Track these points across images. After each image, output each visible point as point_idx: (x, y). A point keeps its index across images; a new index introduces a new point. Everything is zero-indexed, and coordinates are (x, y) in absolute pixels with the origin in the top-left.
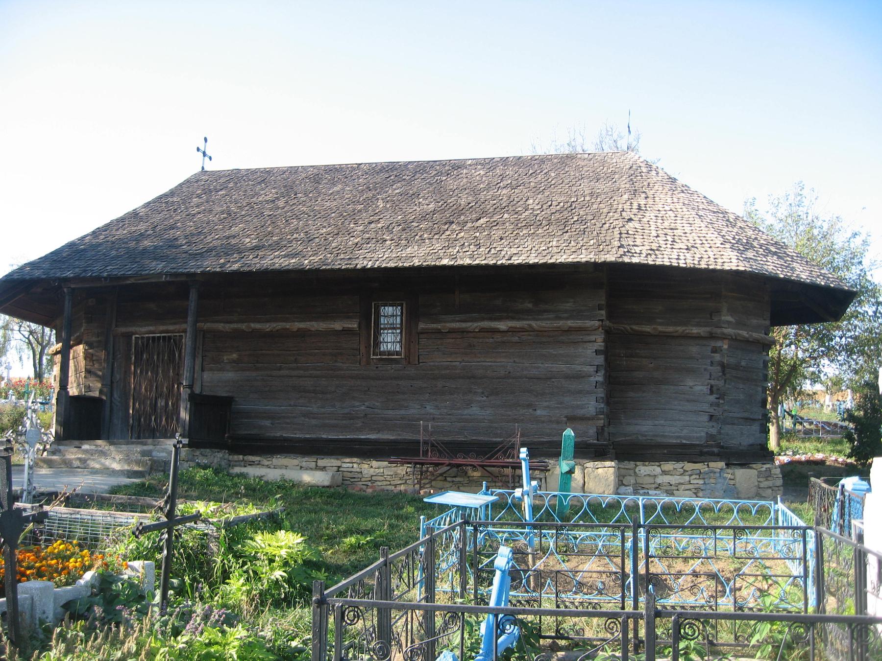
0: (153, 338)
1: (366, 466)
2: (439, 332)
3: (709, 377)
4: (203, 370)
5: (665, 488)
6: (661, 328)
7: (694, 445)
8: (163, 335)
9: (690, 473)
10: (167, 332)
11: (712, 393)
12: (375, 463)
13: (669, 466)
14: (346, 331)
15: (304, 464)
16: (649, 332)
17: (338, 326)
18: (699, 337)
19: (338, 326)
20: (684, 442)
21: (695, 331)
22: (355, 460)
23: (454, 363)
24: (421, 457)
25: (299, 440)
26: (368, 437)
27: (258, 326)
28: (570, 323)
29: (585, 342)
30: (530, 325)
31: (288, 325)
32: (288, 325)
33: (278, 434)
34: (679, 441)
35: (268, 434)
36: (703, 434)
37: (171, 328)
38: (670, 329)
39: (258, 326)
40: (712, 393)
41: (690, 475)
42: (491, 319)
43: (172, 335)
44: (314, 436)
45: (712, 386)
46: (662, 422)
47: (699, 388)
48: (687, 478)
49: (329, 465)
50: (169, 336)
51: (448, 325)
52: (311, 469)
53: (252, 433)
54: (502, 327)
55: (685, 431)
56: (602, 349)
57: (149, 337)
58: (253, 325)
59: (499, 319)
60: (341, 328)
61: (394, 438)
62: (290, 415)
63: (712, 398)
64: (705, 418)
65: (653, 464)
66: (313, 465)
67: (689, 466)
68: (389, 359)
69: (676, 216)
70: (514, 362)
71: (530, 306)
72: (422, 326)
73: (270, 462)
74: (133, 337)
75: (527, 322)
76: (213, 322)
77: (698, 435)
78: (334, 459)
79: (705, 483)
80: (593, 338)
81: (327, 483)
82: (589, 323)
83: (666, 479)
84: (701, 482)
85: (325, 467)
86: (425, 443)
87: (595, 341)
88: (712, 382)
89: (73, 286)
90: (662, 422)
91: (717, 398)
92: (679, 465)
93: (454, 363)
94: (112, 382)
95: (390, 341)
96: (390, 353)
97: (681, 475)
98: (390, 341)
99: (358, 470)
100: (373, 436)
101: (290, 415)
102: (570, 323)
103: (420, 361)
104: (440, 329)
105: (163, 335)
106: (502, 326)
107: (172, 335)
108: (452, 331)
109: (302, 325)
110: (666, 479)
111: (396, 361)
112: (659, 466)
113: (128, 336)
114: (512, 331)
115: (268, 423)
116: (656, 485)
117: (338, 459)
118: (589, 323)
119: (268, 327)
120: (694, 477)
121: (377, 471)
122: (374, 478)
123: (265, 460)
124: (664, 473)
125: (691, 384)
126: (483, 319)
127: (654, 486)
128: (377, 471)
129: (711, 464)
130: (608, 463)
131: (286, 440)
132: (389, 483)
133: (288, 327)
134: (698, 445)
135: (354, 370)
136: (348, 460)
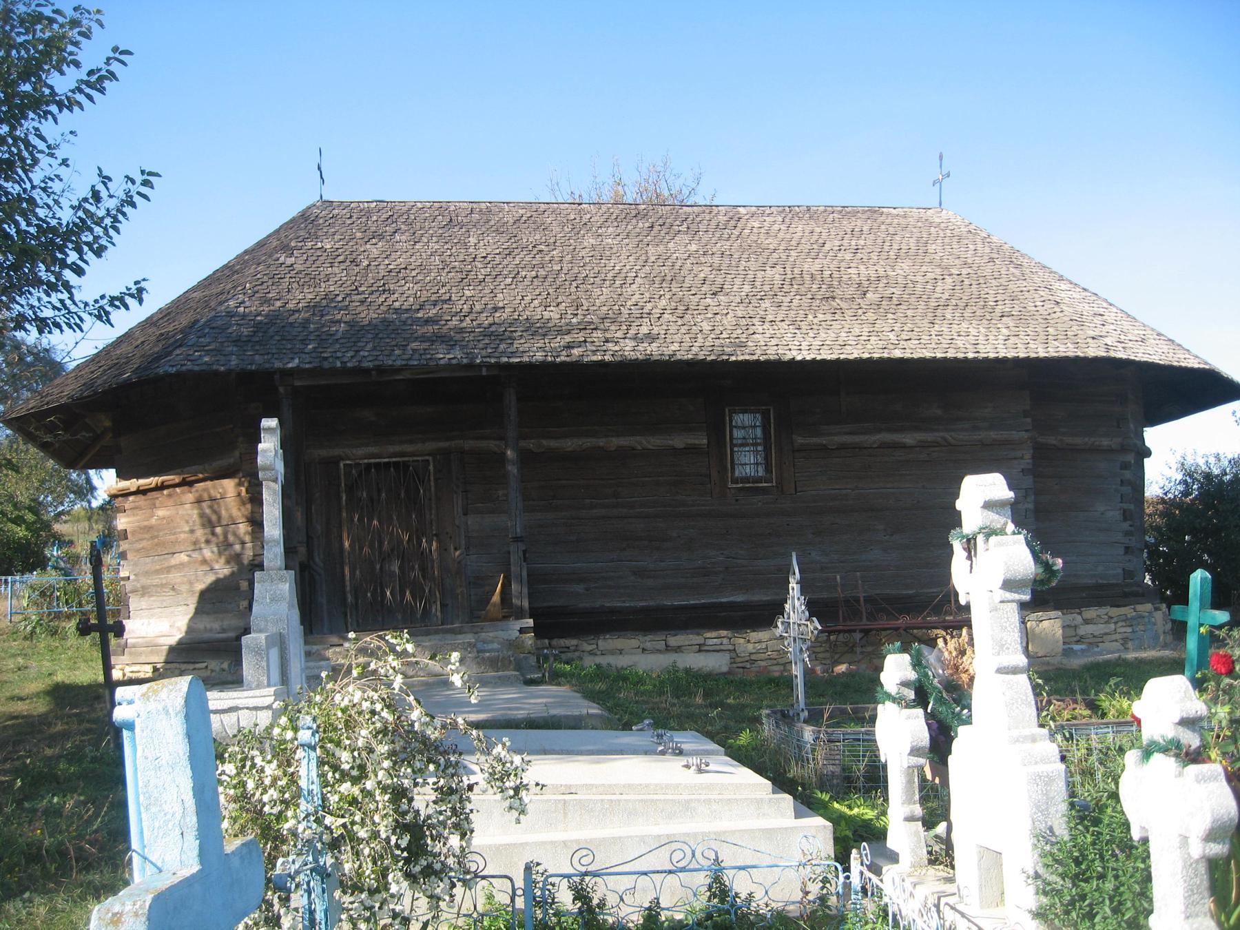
0: (377, 465)
1: (742, 641)
2: (824, 448)
3: (1120, 500)
4: (465, 514)
5: (1087, 640)
6: (1069, 440)
7: (1112, 585)
8: (394, 460)
9: (1115, 620)
10: (402, 455)
11: (1125, 519)
12: (754, 636)
13: (1091, 613)
14: (691, 450)
15: (648, 645)
16: (1054, 445)
17: (679, 441)
18: (1110, 450)
19: (679, 441)
20: (1101, 581)
21: (1105, 442)
22: (724, 633)
23: (844, 492)
24: (864, 621)
25: (636, 611)
26: (731, 599)
27: (553, 444)
28: (993, 435)
29: (1011, 459)
30: (945, 439)
31: (601, 442)
32: (601, 442)
33: (598, 604)
34: (1094, 581)
35: (581, 605)
36: (1120, 571)
37: (409, 448)
38: (1078, 440)
39: (553, 444)
40: (1125, 519)
41: (1116, 623)
42: (889, 430)
43: (411, 459)
44: (652, 603)
45: (1125, 511)
46: (1074, 558)
47: (1110, 514)
48: (1112, 626)
49: (687, 643)
50: (404, 462)
51: (836, 438)
52: (659, 651)
53: (556, 604)
54: (908, 441)
55: (1100, 569)
56: (1031, 467)
57: (370, 464)
58: (544, 442)
59: (901, 430)
60: (682, 446)
61: (769, 598)
62: (612, 574)
63: (1126, 526)
64: (1122, 551)
65: (1073, 611)
66: (662, 645)
67: (1114, 612)
68: (751, 488)
69: (943, 279)
70: (924, 487)
71: (939, 412)
72: (799, 440)
73: (595, 646)
74: (342, 465)
75: (942, 434)
76: (477, 438)
77: (1115, 572)
78: (692, 634)
79: (1133, 632)
80: (1019, 454)
81: (725, 669)
82: (1016, 435)
83: (1090, 629)
84: (1129, 630)
85: (679, 647)
86: (868, 600)
87: (1022, 458)
88: (1125, 506)
89: (298, 383)
90: (1074, 558)
91: (1131, 526)
92: (1102, 611)
93: (844, 492)
94: (309, 537)
95: (748, 463)
96: (746, 479)
97: (1106, 623)
98: (748, 463)
99: (731, 647)
100: (739, 598)
101: (612, 574)
102: (993, 435)
103: (799, 489)
104: (824, 445)
105: (394, 460)
106: (909, 439)
107: (411, 459)
108: (843, 447)
109: (588, 442)
110: (1090, 629)
111: (764, 491)
112: (1080, 614)
113: (335, 461)
114: (923, 445)
115: (579, 588)
116: (1078, 638)
117: (698, 634)
118: (1016, 435)
119: (570, 444)
120: (1120, 624)
121: (758, 646)
122: (753, 657)
123: (585, 644)
124: (1087, 622)
125: (1102, 509)
126: (880, 431)
127: (1075, 639)
128: (758, 646)
129: (1139, 607)
130: (1053, 614)
131: (613, 611)
132: (775, 662)
133: (601, 444)
134: (1117, 585)
135: (703, 505)
136: (714, 634)
